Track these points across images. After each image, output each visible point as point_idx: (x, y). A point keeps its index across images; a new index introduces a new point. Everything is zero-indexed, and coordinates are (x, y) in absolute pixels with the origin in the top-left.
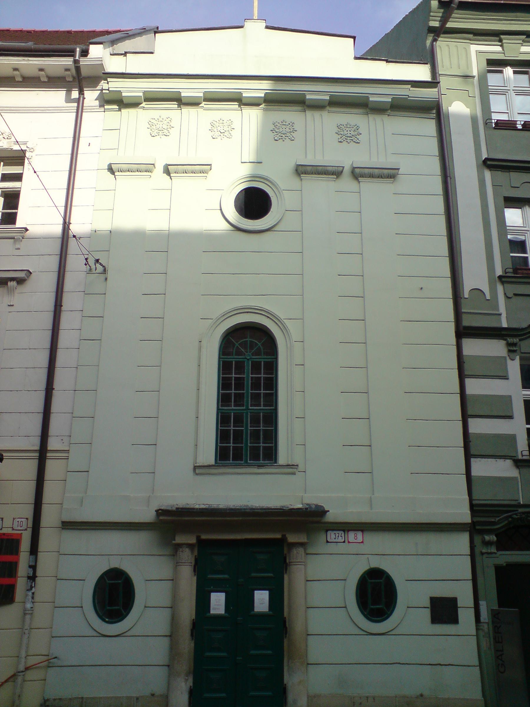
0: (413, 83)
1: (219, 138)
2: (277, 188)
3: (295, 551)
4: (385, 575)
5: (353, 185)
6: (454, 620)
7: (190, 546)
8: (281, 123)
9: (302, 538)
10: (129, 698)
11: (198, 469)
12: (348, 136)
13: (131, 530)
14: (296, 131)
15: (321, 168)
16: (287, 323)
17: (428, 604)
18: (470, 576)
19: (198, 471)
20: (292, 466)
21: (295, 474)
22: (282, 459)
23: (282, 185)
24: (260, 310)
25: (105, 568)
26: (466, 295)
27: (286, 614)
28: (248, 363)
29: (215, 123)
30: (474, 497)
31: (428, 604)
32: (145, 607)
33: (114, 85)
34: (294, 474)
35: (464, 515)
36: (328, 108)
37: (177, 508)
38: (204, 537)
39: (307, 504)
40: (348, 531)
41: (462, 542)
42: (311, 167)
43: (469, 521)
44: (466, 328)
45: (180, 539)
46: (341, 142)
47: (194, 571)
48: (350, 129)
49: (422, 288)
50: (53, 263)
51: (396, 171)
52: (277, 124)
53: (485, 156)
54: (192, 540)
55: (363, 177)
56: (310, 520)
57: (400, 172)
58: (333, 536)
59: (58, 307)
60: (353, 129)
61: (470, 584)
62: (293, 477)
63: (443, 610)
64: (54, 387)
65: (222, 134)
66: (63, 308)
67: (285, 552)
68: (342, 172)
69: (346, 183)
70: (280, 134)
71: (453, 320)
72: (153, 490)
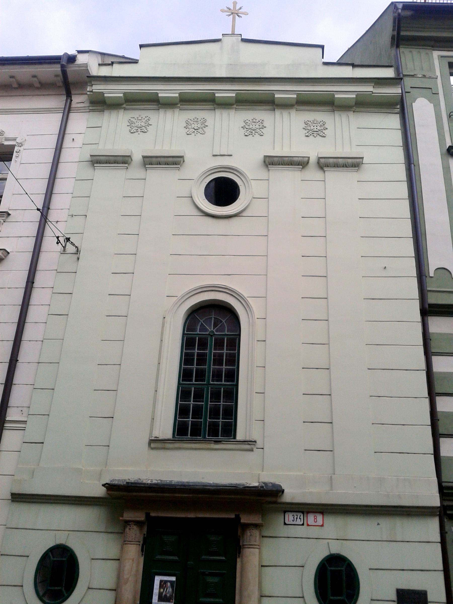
0: (377, 80)
1: (193, 134)
2: (245, 177)
4: (347, 562)
5: (319, 175)
7: (139, 524)
8: (251, 121)
9: (255, 519)
11: (156, 443)
12: (317, 132)
13: (81, 504)
14: (265, 127)
15: (287, 158)
16: (248, 299)
17: (394, 597)
18: (441, 567)
19: (153, 445)
20: (250, 443)
21: (253, 451)
22: (240, 436)
23: (250, 175)
24: (225, 288)
25: (51, 544)
26: (432, 274)
28: (211, 340)
29: (189, 121)
30: (444, 479)
32: (89, 588)
33: (97, 88)
34: (252, 450)
35: (435, 501)
36: (296, 106)
37: (127, 483)
38: (153, 514)
39: (264, 483)
40: (308, 513)
41: (431, 528)
42: (277, 159)
43: (438, 504)
44: (431, 305)
45: (128, 515)
46: (307, 136)
47: (142, 551)
48: (316, 125)
49: (385, 268)
50: (30, 244)
51: (361, 160)
52: (247, 121)
53: (449, 143)
54: (140, 516)
55: (328, 167)
56: (265, 501)
57: (365, 161)
58: (291, 518)
59: (30, 284)
60: (319, 125)
61: (441, 576)
62: (251, 453)
64: (18, 359)
65: (196, 131)
66: (35, 285)
67: (239, 533)
68: (308, 163)
69: (312, 173)
70: (250, 130)
71: (418, 298)
72: (106, 464)
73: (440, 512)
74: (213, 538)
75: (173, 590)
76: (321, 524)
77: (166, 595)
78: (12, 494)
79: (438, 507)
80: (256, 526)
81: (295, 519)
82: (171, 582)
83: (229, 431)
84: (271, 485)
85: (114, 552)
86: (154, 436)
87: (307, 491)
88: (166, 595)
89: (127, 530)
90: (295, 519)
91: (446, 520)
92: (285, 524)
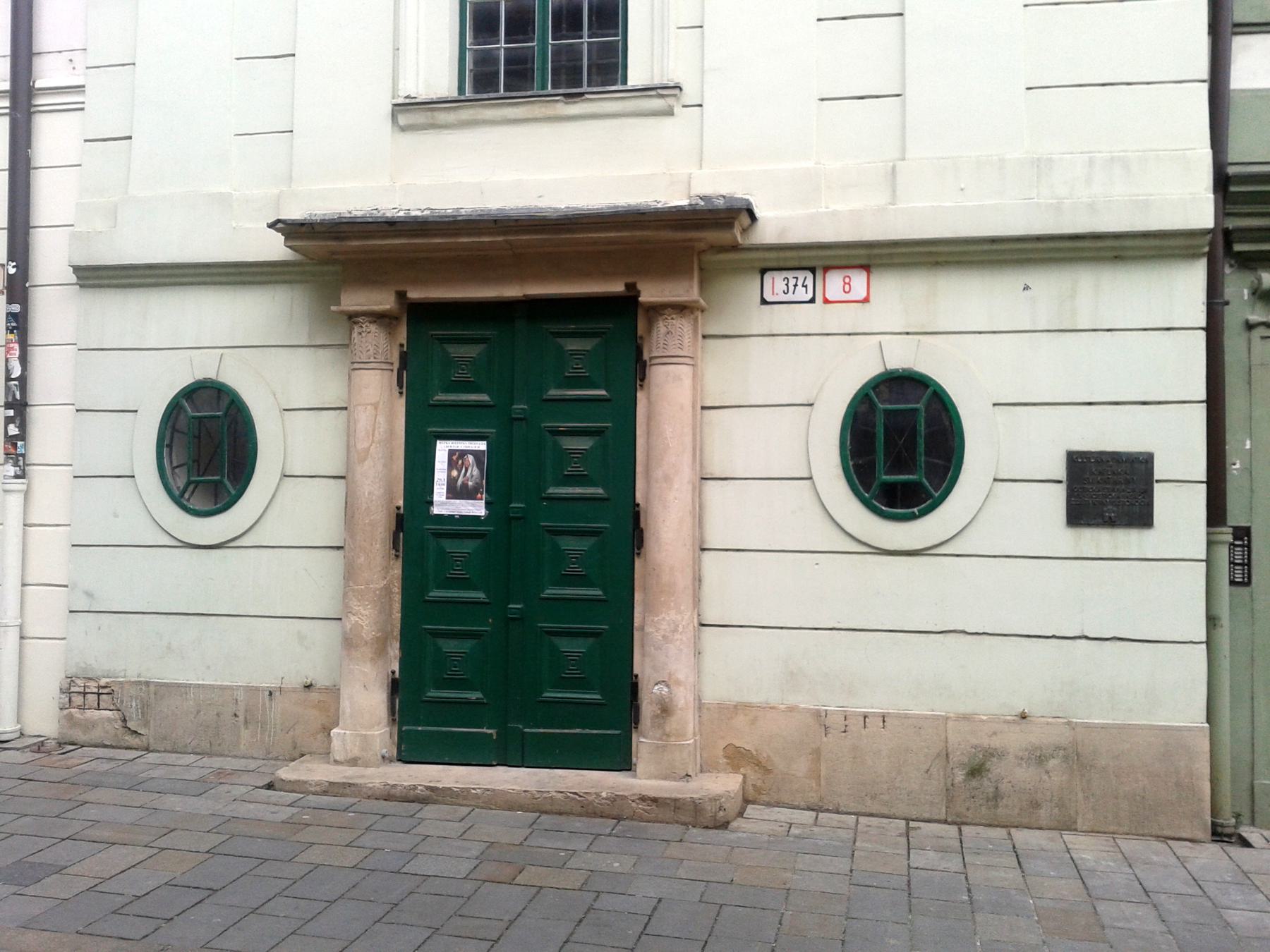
3: (661, 327)
4: (929, 391)
6: (1138, 514)
7: (379, 318)
10: (252, 690)
11: (412, 113)
19: (403, 120)
22: (636, 76)
27: (639, 497)
31: (1059, 469)
32: (995, 480)
34: (669, 113)
35: (1196, 209)
38: (414, 294)
40: (826, 269)
43: (1209, 223)
45: (354, 300)
47: (400, 384)
54: (384, 301)
56: (704, 242)
61: (1199, 415)
62: (667, 122)
63: (1107, 491)
67: (641, 329)
73: (1212, 244)
74: (572, 345)
75: (481, 470)
76: (864, 295)
77: (464, 485)
78: (77, 269)
79: (1208, 231)
80: (682, 309)
81: (791, 288)
82: (475, 453)
83: (609, 68)
84: (722, 201)
85: (333, 392)
86: (403, 93)
87: (824, 210)
88: (464, 485)
89: (355, 335)
90: (791, 288)
91: (1227, 270)
92: (764, 302)
